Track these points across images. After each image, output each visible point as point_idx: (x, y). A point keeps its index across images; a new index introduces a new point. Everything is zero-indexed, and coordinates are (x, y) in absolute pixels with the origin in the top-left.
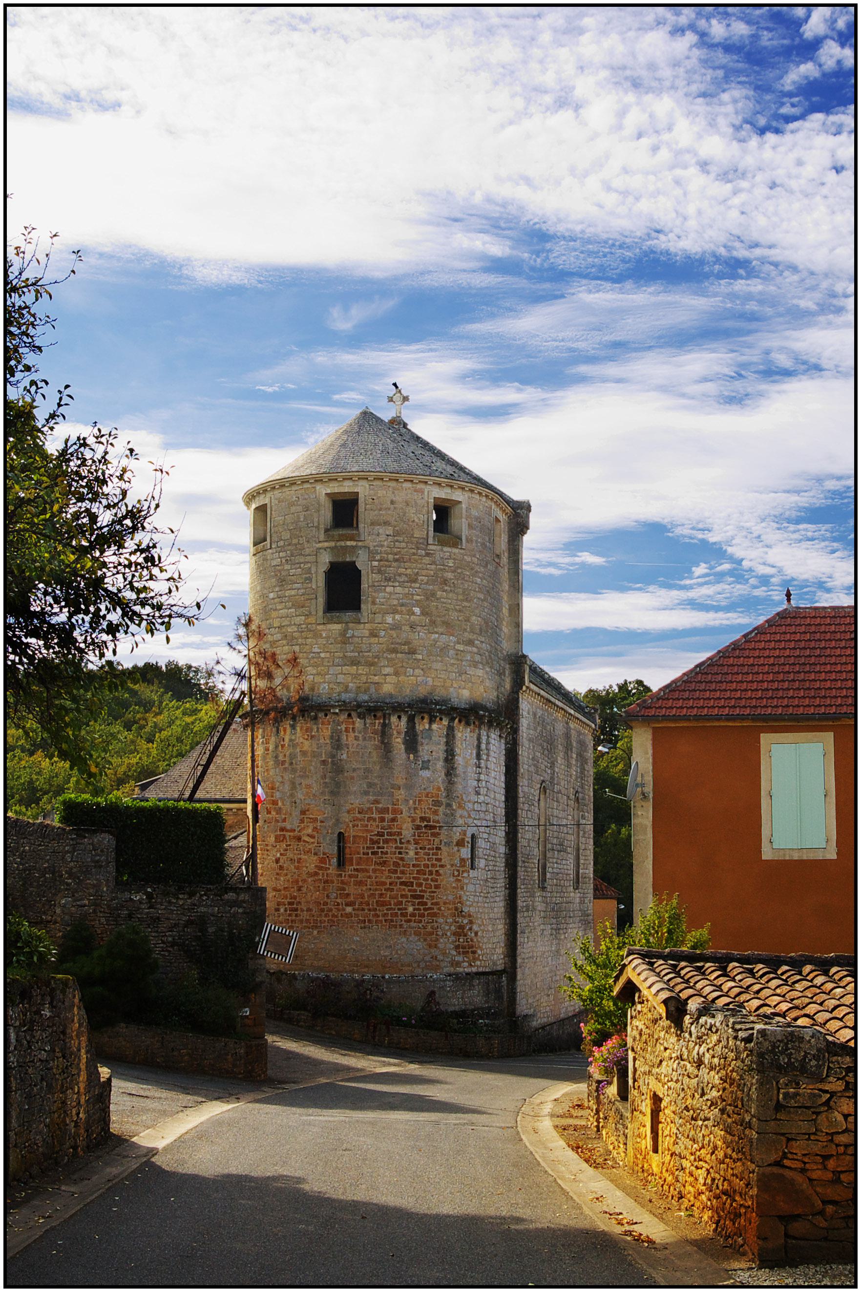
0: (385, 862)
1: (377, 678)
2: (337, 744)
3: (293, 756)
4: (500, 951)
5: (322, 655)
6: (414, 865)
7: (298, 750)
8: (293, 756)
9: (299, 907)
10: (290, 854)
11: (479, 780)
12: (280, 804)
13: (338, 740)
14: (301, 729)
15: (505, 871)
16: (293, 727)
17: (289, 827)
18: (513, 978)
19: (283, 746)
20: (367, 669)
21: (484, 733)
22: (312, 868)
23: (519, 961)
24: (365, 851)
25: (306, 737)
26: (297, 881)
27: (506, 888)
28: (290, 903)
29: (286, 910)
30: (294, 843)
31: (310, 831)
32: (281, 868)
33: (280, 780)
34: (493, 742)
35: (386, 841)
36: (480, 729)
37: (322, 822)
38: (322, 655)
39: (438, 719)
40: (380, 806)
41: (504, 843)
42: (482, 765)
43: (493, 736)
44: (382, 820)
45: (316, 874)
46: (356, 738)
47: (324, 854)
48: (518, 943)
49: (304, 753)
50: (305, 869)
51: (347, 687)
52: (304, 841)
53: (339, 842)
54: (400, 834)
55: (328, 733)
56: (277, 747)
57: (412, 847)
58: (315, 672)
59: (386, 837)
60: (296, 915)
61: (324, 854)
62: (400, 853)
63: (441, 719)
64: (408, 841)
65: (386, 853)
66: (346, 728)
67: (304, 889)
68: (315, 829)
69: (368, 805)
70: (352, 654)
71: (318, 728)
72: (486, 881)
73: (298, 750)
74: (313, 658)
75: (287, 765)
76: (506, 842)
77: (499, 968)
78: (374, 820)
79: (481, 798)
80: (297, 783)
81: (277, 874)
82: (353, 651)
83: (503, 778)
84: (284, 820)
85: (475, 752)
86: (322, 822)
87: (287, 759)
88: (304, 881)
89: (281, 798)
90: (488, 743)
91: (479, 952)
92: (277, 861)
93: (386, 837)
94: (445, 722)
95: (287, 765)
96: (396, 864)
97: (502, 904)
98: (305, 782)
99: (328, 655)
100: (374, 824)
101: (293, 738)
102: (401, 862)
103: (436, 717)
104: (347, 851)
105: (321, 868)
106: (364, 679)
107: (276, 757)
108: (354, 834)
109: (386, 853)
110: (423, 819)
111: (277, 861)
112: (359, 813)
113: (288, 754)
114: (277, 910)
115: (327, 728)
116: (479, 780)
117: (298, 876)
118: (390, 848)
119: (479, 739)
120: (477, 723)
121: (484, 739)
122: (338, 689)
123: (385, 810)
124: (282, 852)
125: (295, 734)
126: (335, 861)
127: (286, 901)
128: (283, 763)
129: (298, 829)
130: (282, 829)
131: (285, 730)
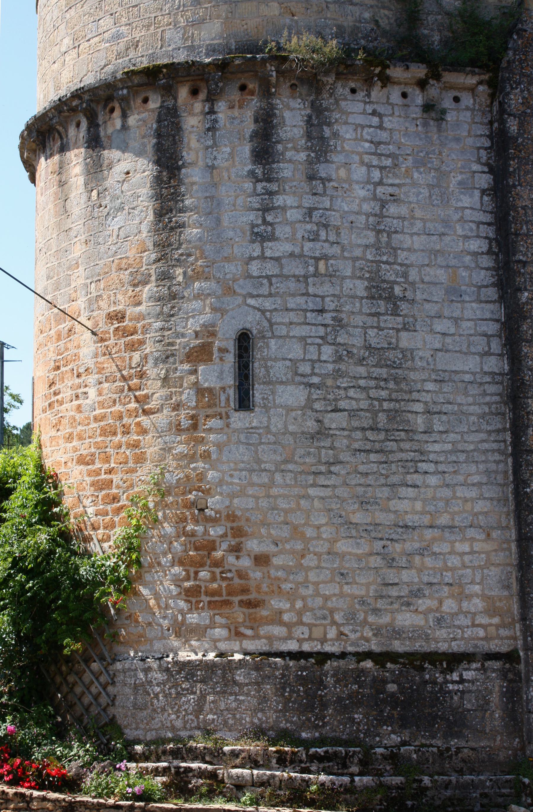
6: (96, 419)
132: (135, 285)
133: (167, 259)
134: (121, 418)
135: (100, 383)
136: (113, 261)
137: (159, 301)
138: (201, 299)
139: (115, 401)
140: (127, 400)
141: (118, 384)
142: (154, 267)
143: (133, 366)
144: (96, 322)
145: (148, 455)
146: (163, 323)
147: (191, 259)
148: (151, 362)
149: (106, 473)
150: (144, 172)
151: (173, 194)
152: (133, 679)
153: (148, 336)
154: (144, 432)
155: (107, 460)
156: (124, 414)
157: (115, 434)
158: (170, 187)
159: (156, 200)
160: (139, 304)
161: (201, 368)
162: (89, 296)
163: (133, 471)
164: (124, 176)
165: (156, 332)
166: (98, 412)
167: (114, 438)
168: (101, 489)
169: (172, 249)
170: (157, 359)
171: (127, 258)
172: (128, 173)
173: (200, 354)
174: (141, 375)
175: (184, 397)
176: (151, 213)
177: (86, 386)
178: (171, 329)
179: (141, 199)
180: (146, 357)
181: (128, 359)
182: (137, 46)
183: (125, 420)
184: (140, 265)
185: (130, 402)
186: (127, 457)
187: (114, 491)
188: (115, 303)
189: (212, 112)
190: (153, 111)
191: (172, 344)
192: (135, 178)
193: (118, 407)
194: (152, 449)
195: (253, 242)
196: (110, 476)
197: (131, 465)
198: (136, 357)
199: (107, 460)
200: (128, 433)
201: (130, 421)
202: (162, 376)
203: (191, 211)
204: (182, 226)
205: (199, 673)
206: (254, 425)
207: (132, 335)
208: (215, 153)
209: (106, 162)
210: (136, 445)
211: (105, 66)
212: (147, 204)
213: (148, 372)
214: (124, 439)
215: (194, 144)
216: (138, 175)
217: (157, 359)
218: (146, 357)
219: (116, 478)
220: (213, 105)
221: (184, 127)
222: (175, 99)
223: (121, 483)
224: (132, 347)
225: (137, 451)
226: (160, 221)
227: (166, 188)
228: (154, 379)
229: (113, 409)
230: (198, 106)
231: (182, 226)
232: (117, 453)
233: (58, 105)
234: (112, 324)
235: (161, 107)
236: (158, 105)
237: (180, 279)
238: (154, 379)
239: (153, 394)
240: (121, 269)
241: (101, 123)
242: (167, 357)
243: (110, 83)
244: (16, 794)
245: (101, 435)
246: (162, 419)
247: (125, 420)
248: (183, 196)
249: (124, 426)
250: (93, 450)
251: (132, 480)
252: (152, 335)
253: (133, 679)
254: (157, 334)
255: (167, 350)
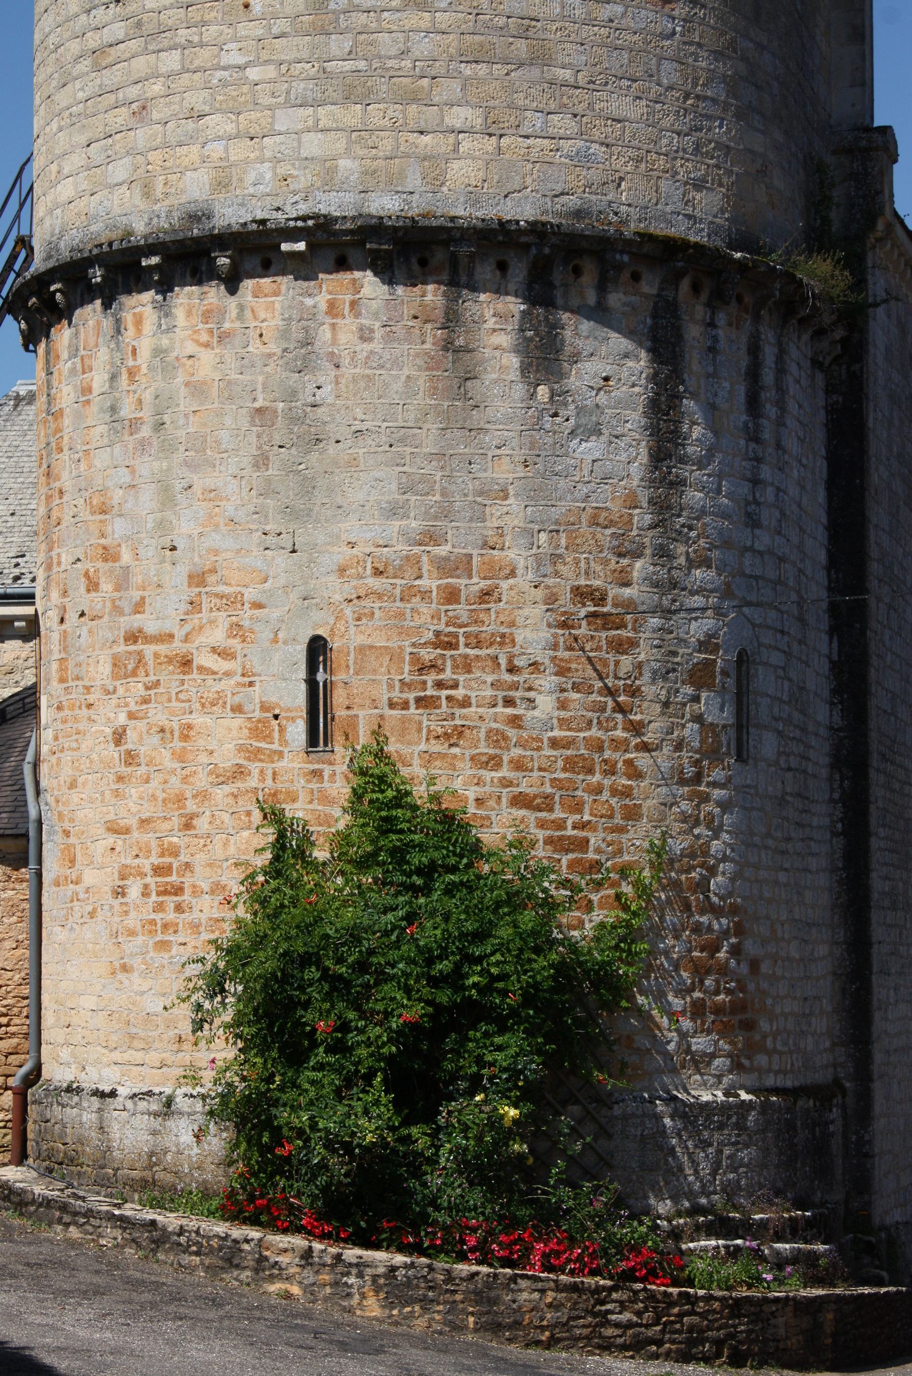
0: (460, 731)
1: (426, 139)
2: (303, 353)
3: (163, 402)
4: (820, 1024)
5: (253, 74)
6: (554, 743)
7: (180, 380)
8: (163, 402)
9: (188, 880)
10: (157, 715)
11: (756, 482)
12: (126, 557)
13: (307, 343)
14: (189, 313)
15: (830, 779)
16: (164, 310)
17: (151, 627)
18: (863, 1114)
19: (132, 373)
20: (395, 111)
21: (768, 335)
22: (227, 756)
23: (878, 1057)
24: (396, 695)
25: (204, 337)
26: (180, 799)
27: (834, 834)
28: (159, 871)
29: (145, 894)
30: (170, 678)
31: (218, 636)
32: (130, 758)
33: (124, 476)
34: (793, 369)
35: (467, 666)
36: (757, 318)
37: (258, 606)
38: (253, 74)
39: (626, 275)
40: (442, 550)
41: (826, 694)
42: (766, 435)
43: (794, 353)
44: (452, 596)
45: (239, 772)
46: (365, 335)
47: (264, 708)
48: (875, 1003)
49: (197, 389)
50: (203, 758)
51: (332, 171)
52: (201, 669)
53: (312, 668)
54: (505, 640)
55: (273, 323)
56: (114, 377)
57: (548, 681)
58: (230, 128)
59: (462, 650)
60: (179, 908)
61: (264, 708)
62: (509, 702)
63: (636, 277)
64: (534, 665)
65: (465, 703)
66: (332, 305)
67: (202, 824)
68: (236, 630)
69: (403, 548)
70: (348, 65)
71: (241, 308)
72: (782, 802)
73: (180, 380)
74: (224, 83)
75: (145, 431)
76: (834, 692)
77: (821, 1077)
78: (425, 595)
79: (764, 540)
80: (178, 486)
81: (120, 779)
82: (351, 55)
83: (821, 496)
84: (139, 607)
85: (741, 391)
86: (258, 606)
87: (146, 414)
88: (203, 796)
89: (128, 538)
90: (781, 371)
91: (764, 1025)
92: (119, 737)
93: (462, 650)
94: (649, 286)
95: (145, 431)
96: (497, 738)
97: (823, 880)
98: (200, 482)
99: (270, 72)
100: (424, 609)
101: (165, 342)
102: (512, 733)
103: (619, 267)
104: (339, 697)
105: (255, 754)
106: (386, 145)
107: (113, 409)
108: (361, 640)
109: (465, 703)
110: (581, 594)
111: (119, 737)
112: (378, 572)
113: (148, 397)
114: (120, 892)
115: (270, 307)
116: (756, 482)
117: (185, 780)
118: (478, 686)
119: (754, 350)
120: (748, 299)
121: (769, 353)
122: (303, 179)
123: (462, 565)
124: (133, 707)
125: (171, 329)
126: (298, 731)
127: (146, 864)
128: (134, 425)
129: (179, 634)
130: (133, 637)
131: (139, 321)
132: (621, 555)
133: (666, 527)
134: (601, 749)
135: (563, 690)
136: (584, 509)
137: (656, 587)
138: (704, 596)
139: (590, 723)
140: (612, 724)
141: (594, 697)
142: (650, 533)
143: (621, 675)
144: (553, 594)
145: (644, 810)
146: (663, 621)
147: (693, 534)
148: (647, 676)
149: (574, 828)
150: (633, 386)
151: (672, 432)
152: (639, 1129)
153: (641, 635)
154: (638, 775)
155: (578, 808)
156: (606, 745)
157: (591, 771)
158: (670, 421)
159: (650, 435)
160: (627, 584)
161: (704, 695)
162: (534, 551)
163: (621, 830)
164: (602, 383)
165: (654, 631)
166: (556, 733)
167: (589, 777)
168: (567, 851)
169: (673, 515)
170: (655, 672)
171: (607, 509)
172: (606, 379)
173: (701, 676)
174: (634, 692)
175: (687, 732)
176: (643, 451)
177: (530, 689)
178: (671, 632)
179: (629, 425)
180: (640, 666)
181: (612, 664)
182: (619, 185)
183: (607, 754)
184: (629, 527)
185: (615, 728)
186: (612, 808)
187: (591, 855)
188: (587, 573)
189: (712, 325)
190: (646, 296)
191: (674, 654)
192: (621, 392)
193: (594, 732)
194: (650, 803)
195: (747, 526)
196: (584, 834)
197: (618, 820)
198: (626, 662)
199: (578, 808)
200: (613, 774)
201: (616, 755)
202: (663, 698)
203: (693, 465)
204: (683, 482)
205: (716, 1118)
206: (748, 782)
207: (617, 629)
208: (716, 386)
209: (568, 349)
210: (626, 793)
211: (562, 194)
212: (637, 437)
213: (643, 688)
214: (607, 782)
215: (695, 367)
216: (624, 388)
217: (655, 672)
218: (640, 666)
219: (594, 840)
220: (713, 313)
221: (686, 336)
222: (677, 290)
223: (603, 846)
224: (621, 647)
225: (627, 801)
226: (656, 468)
227: (665, 421)
228: (651, 701)
229: (587, 734)
230: (700, 311)
231: (683, 482)
232: (595, 800)
233: (492, 230)
234: (584, 605)
235: (658, 295)
236: (654, 291)
237: (682, 560)
238: (651, 701)
239: (650, 722)
240: (598, 524)
241: (557, 283)
242: (668, 672)
243: (609, 239)
244: (680, 1293)
245: (564, 770)
246: (664, 758)
247: (607, 754)
248: (685, 439)
249: (605, 761)
250: (549, 790)
251: (621, 843)
252: (648, 635)
253: (639, 1129)
254: (655, 636)
255: (668, 662)
